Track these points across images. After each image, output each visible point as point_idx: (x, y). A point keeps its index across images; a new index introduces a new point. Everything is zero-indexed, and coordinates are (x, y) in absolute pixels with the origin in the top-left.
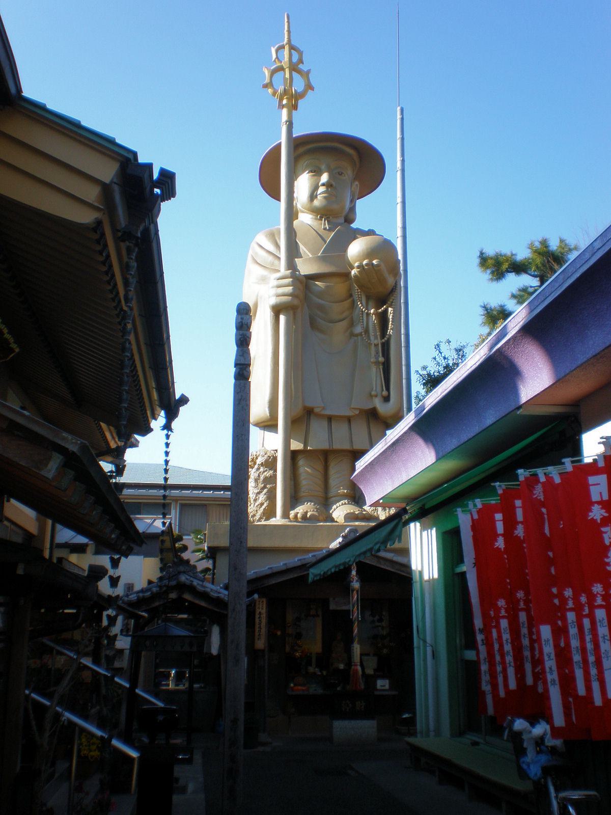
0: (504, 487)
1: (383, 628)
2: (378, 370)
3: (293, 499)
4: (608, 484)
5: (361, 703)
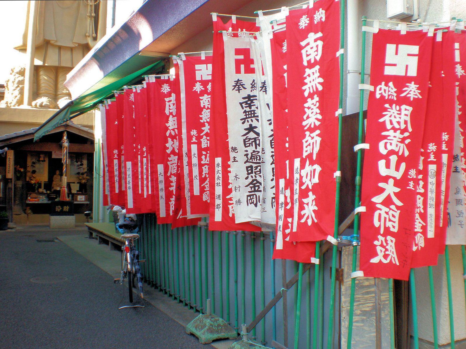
0: (118, 93)
1: (84, 169)
2: (91, 22)
3: (35, 94)
4: (99, 89)
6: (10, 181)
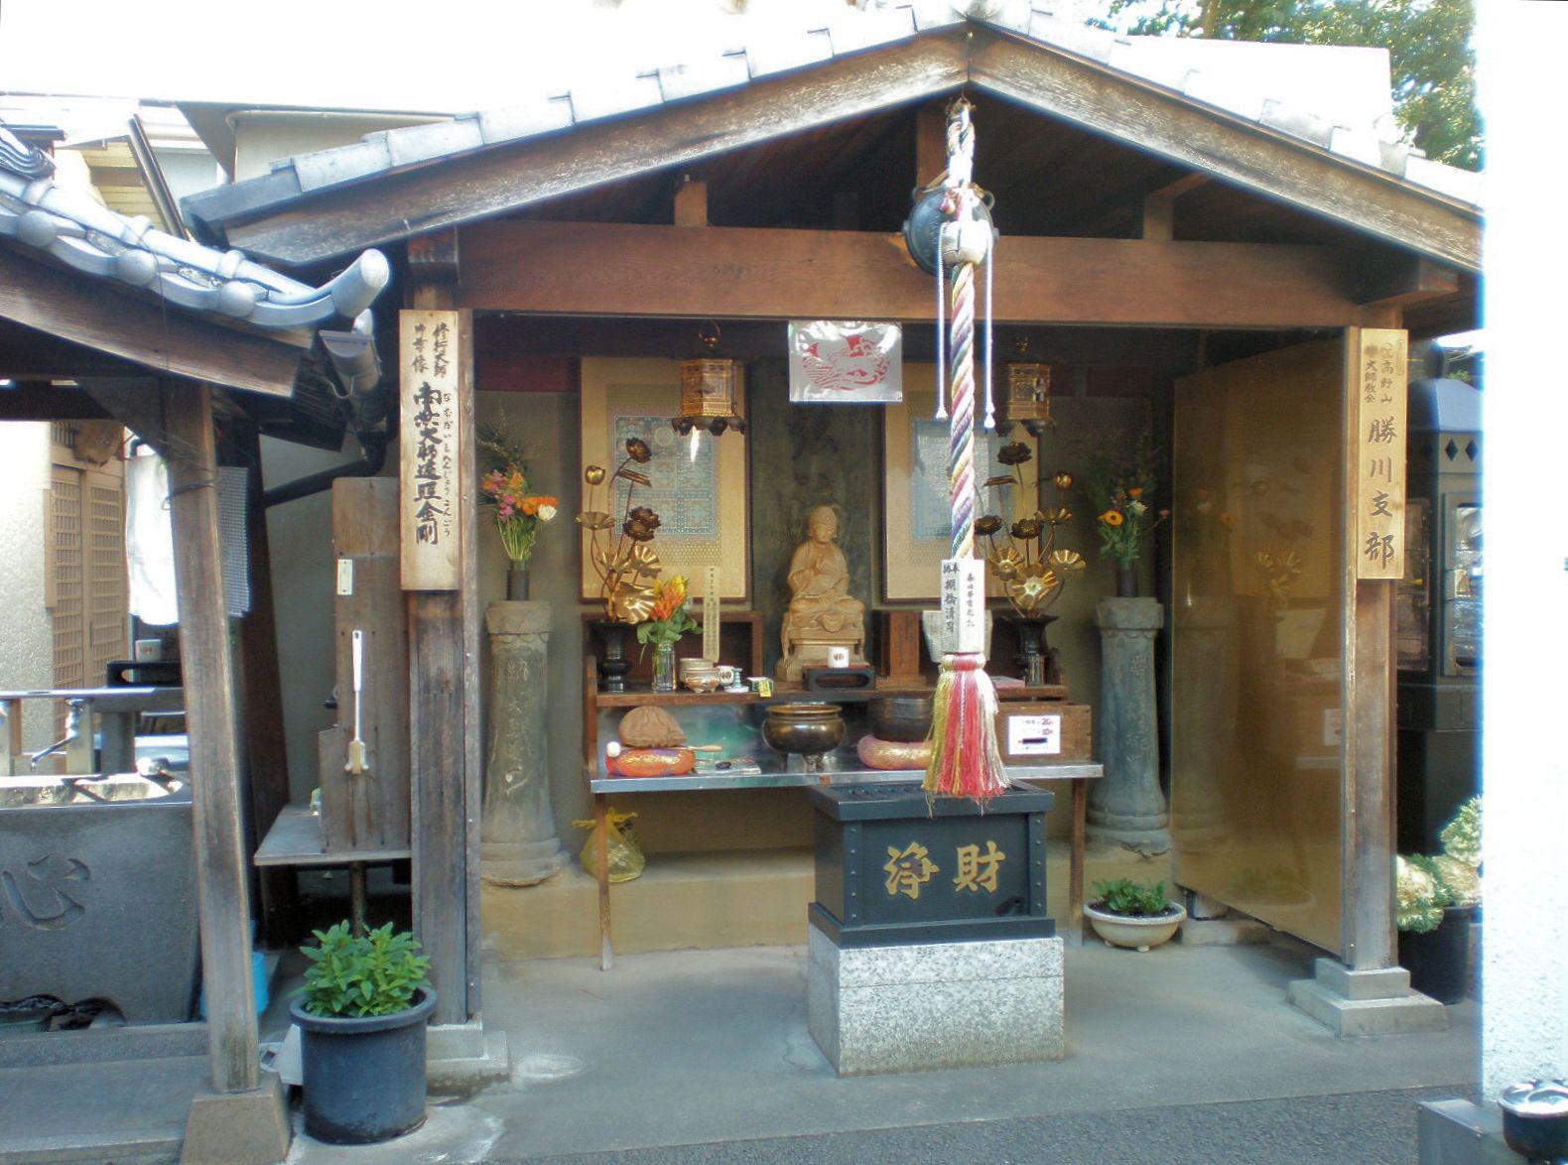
5: (984, 851)
6: (435, 611)
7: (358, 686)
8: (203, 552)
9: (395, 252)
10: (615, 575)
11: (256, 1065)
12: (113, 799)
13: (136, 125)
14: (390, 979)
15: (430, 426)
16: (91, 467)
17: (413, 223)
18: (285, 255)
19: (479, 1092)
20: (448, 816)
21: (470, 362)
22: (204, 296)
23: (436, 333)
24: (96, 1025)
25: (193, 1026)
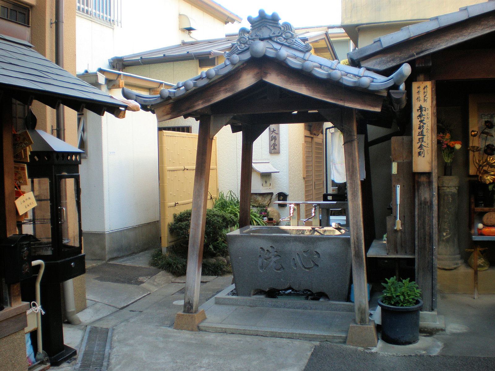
7: (398, 203)
8: (353, 161)
9: (412, 63)
10: (481, 167)
11: (368, 318)
12: (325, 234)
13: (326, 34)
14: (409, 296)
15: (422, 119)
16: (315, 136)
17: (417, 54)
18: (378, 68)
19: (435, 334)
20: (427, 245)
21: (435, 97)
22: (355, 82)
23: (424, 88)
24: (321, 300)
25: (348, 303)
